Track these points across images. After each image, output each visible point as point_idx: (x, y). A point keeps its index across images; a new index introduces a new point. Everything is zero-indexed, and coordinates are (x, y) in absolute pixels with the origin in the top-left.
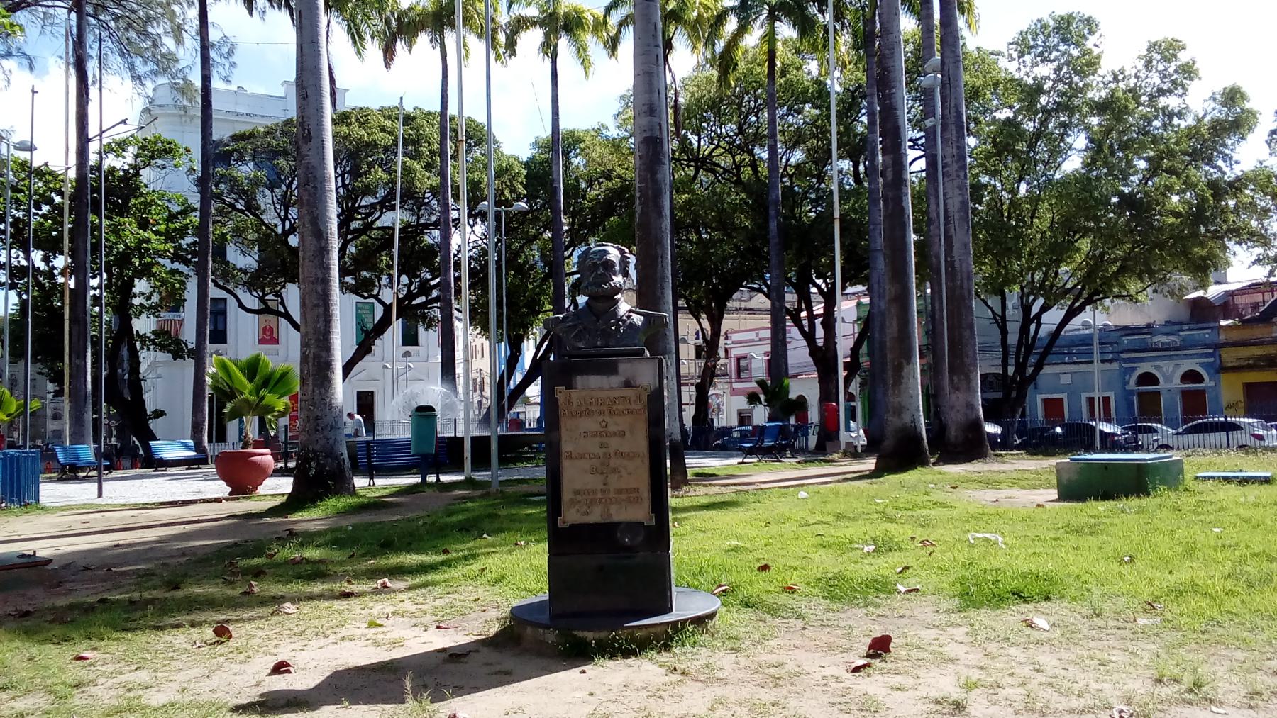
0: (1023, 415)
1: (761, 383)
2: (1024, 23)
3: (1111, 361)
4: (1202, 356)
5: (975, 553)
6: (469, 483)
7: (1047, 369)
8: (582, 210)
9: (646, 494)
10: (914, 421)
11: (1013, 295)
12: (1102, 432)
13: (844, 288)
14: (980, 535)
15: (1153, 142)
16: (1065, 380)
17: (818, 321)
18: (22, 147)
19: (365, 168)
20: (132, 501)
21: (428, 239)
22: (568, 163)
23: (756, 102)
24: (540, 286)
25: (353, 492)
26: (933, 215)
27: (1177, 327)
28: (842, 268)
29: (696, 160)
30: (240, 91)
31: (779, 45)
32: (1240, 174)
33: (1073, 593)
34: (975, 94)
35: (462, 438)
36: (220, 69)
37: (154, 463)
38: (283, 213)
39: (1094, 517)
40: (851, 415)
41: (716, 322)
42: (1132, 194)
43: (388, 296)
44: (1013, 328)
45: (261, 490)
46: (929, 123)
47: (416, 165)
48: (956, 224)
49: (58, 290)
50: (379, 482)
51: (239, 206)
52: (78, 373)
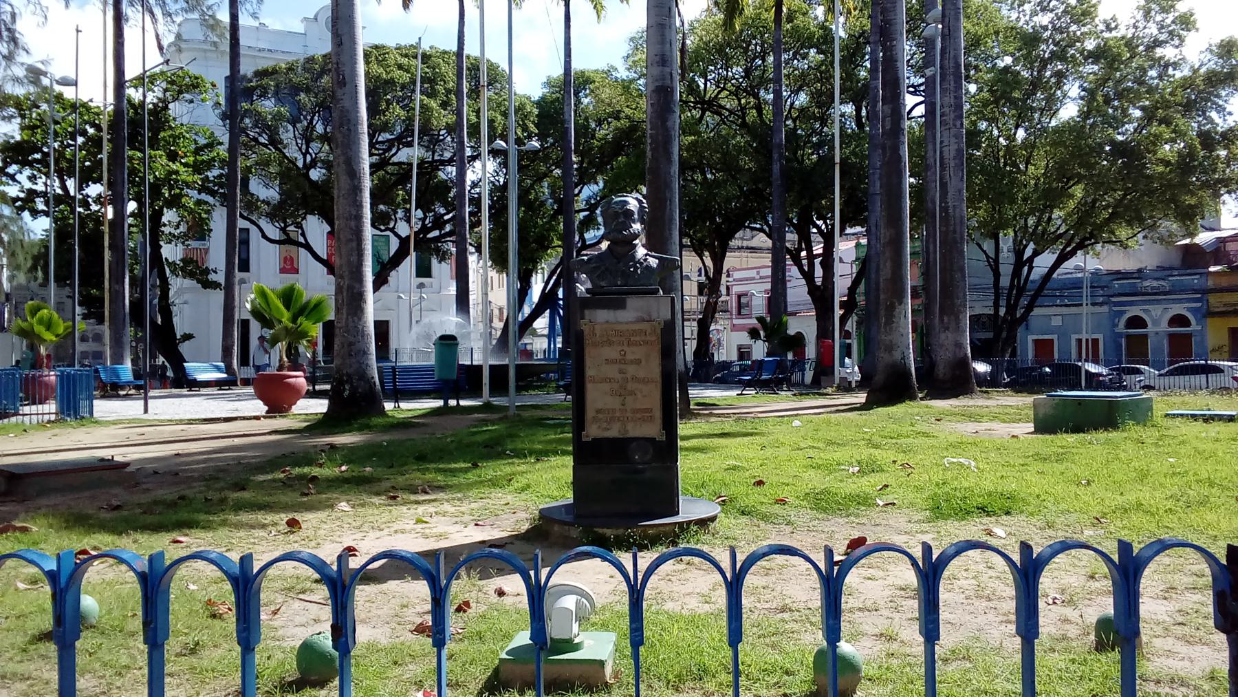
0: (1013, 354)
1: (761, 320)
3: (1101, 304)
6: (487, 407)
7: (1037, 311)
8: (592, 149)
9: (658, 414)
10: (903, 358)
11: (1007, 240)
12: (1087, 371)
13: (842, 229)
15: (1147, 92)
16: (1056, 322)
17: (817, 261)
18: (65, 82)
20: (177, 417)
22: (578, 102)
23: (762, 46)
24: (549, 222)
25: (382, 412)
29: (703, 102)
32: (1233, 124)
33: (1031, 509)
34: (975, 42)
35: (480, 367)
36: (248, 6)
37: (184, 382)
39: (1062, 447)
41: (718, 260)
43: (403, 229)
44: (1006, 270)
45: (295, 409)
46: (928, 72)
48: (950, 171)
49: (98, 219)
50: (404, 405)
51: (263, 141)
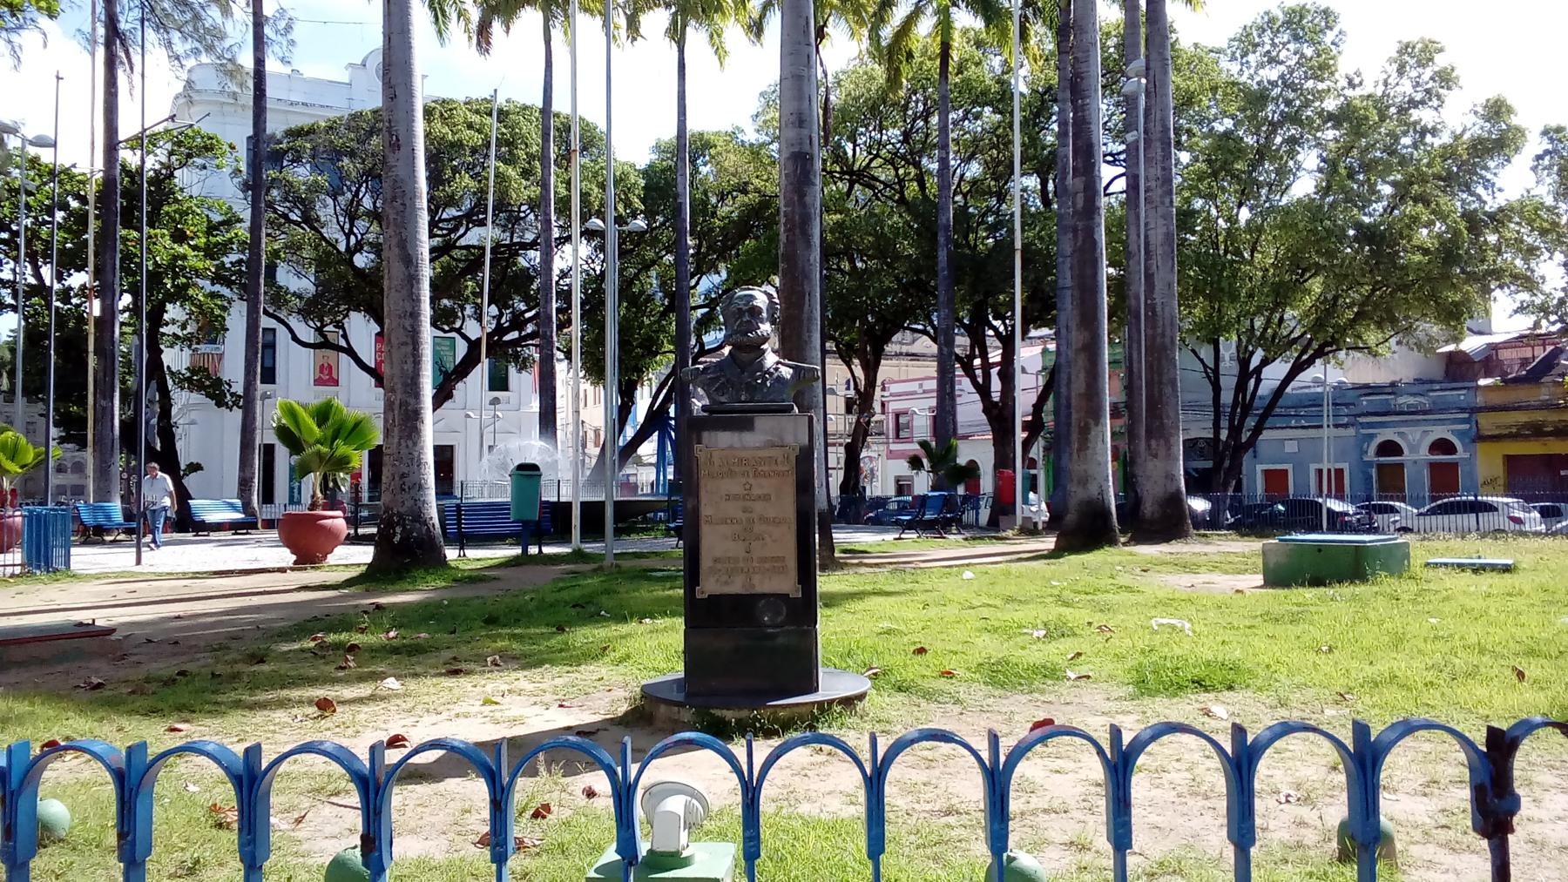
0: (1238, 488)
2: (1250, 15)
3: (1345, 426)
4: (1456, 421)
5: (1157, 639)
6: (578, 556)
9: (792, 563)
12: (1329, 510)
13: (1025, 332)
14: (1165, 621)
15: (1400, 163)
16: (1291, 447)
17: (994, 371)
18: (40, 142)
19: (449, 172)
20: (179, 570)
21: (522, 262)
22: (695, 171)
26: (1133, 248)
27: (1427, 386)
28: (1023, 308)
29: (851, 172)
30: (295, 75)
31: (956, 35)
33: (1259, 683)
34: (1188, 100)
35: (570, 504)
36: (276, 48)
38: (347, 226)
39: (1298, 605)
40: (1032, 484)
41: (871, 369)
42: (1369, 226)
43: (473, 330)
44: (1228, 383)
45: (332, 559)
46: (1130, 137)
47: (511, 172)
48: (1158, 259)
50: (471, 553)
52: (104, 415)
